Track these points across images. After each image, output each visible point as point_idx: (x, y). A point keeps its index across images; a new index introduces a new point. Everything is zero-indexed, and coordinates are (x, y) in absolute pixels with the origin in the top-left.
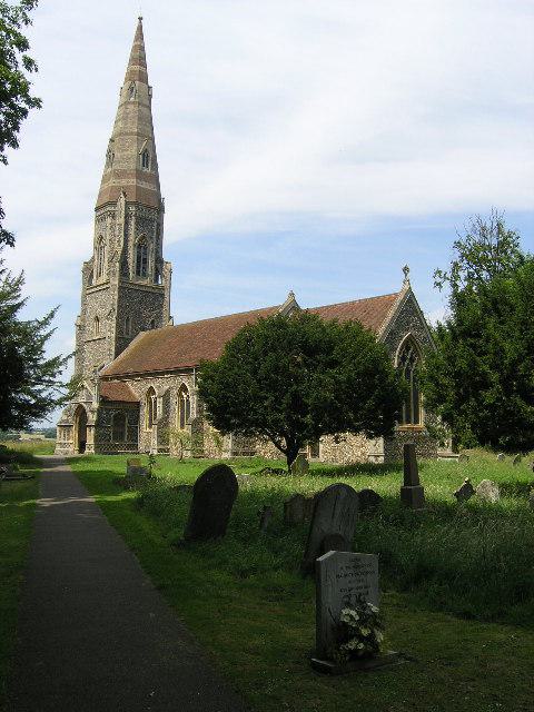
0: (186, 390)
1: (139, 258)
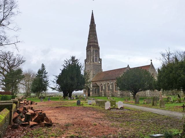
0: (102, 85)
1: (96, 58)
